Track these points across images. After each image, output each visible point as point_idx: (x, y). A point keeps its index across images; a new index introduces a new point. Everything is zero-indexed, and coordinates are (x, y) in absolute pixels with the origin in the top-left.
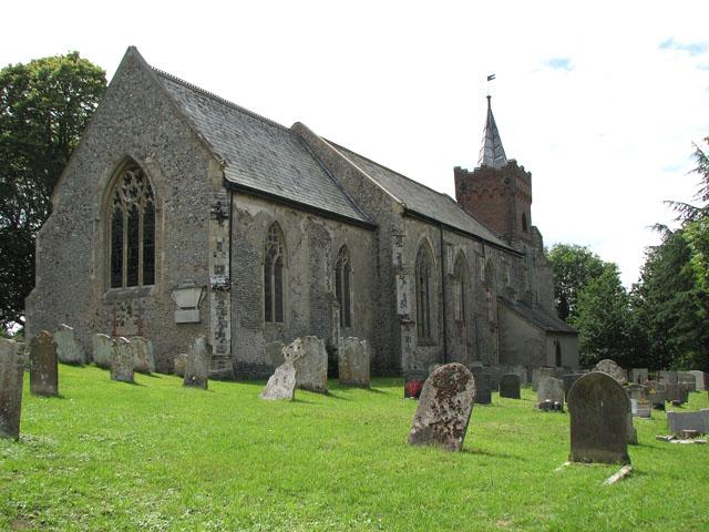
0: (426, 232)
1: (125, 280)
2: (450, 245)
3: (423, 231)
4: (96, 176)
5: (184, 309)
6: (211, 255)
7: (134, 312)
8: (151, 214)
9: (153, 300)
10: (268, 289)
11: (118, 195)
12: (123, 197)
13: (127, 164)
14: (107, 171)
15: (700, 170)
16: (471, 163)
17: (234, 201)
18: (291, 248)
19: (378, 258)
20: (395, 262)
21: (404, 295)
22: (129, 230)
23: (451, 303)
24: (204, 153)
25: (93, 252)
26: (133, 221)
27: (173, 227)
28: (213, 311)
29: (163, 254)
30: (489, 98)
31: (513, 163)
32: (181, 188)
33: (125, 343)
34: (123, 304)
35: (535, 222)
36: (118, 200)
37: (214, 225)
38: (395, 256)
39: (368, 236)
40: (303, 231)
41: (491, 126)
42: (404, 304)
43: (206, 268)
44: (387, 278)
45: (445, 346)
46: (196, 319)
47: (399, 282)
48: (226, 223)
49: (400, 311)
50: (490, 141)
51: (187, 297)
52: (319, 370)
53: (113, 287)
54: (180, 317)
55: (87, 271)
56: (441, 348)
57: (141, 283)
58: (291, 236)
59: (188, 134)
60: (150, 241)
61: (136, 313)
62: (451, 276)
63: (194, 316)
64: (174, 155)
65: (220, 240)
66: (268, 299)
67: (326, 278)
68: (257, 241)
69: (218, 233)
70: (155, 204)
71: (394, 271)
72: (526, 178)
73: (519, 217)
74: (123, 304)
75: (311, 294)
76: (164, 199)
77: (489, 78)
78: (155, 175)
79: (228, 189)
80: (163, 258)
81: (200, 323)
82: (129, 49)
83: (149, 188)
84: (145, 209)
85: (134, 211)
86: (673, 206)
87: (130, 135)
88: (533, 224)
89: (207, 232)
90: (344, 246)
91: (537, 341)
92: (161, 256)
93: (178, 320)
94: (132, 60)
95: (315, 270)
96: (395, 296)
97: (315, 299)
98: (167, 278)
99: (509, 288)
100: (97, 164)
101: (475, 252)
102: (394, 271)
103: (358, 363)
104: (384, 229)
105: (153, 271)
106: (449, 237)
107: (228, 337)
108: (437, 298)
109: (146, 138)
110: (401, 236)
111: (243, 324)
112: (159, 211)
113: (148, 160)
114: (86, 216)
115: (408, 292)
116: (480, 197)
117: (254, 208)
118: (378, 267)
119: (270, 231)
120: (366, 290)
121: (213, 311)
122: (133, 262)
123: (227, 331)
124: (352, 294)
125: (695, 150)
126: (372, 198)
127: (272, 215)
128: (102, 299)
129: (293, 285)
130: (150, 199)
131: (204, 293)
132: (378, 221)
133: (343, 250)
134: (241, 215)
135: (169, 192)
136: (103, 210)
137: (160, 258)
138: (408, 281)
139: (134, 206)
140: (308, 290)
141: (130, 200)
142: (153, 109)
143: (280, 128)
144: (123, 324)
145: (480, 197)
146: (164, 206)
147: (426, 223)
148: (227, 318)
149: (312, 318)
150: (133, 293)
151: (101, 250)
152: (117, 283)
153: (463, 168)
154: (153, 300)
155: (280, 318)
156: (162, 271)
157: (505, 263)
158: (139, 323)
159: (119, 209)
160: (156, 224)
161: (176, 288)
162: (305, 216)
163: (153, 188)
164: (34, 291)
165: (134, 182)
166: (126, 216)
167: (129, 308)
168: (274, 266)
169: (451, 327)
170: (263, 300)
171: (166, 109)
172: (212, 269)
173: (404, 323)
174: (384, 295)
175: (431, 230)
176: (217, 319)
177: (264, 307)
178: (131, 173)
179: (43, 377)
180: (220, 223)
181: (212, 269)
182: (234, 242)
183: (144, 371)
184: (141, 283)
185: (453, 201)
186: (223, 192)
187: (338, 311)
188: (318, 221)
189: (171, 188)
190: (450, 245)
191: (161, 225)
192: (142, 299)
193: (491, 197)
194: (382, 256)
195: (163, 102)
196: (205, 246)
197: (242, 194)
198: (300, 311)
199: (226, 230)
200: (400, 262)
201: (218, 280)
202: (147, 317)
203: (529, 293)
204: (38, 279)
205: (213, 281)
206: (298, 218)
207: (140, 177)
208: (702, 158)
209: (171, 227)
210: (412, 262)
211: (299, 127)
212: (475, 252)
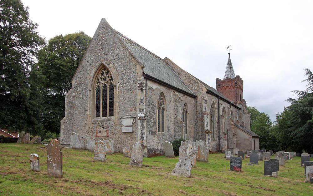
0: (214, 99)
2: (221, 104)
3: (213, 98)
5: (126, 126)
6: (138, 104)
7: (105, 127)
8: (112, 89)
9: (113, 122)
10: (159, 119)
11: (98, 80)
13: (102, 68)
14: (94, 70)
15: (310, 79)
16: (222, 78)
17: (147, 83)
18: (168, 103)
19: (197, 108)
20: (204, 110)
21: (207, 122)
22: (103, 94)
23: (221, 126)
24: (135, 62)
26: (105, 91)
27: (121, 92)
28: (139, 128)
29: (117, 104)
30: (229, 54)
31: (238, 77)
32: (125, 76)
33: (101, 143)
34: (100, 124)
35: (244, 98)
36: (99, 82)
38: (204, 108)
39: (193, 100)
40: (172, 97)
41: (230, 63)
43: (135, 110)
45: (219, 141)
47: (205, 117)
48: (144, 91)
49: (206, 128)
51: (129, 122)
53: (96, 117)
54: (124, 130)
55: (86, 110)
56: (217, 142)
58: (168, 98)
59: (128, 54)
60: (111, 99)
62: (222, 116)
63: (130, 129)
64: (122, 63)
65: (142, 98)
66: (159, 123)
67: (181, 115)
68: (156, 99)
69: (141, 95)
70: (114, 83)
71: (203, 114)
72: (242, 82)
73: (239, 96)
74: (100, 124)
75: (174, 121)
76: (118, 81)
78: (113, 72)
79: (145, 78)
80: (117, 106)
81: (133, 132)
82: (102, 19)
83: (111, 77)
84: (110, 86)
85: (105, 87)
87: (103, 55)
88: (243, 99)
89: (136, 95)
90: (186, 103)
91: (248, 140)
92: (116, 105)
94: (104, 26)
95: (176, 112)
96: (204, 123)
97: (176, 123)
98: (119, 114)
99: (237, 120)
100: (89, 67)
101: (228, 107)
102: (203, 114)
103: (203, 152)
104: (199, 98)
105: (113, 111)
106: (221, 102)
107: (145, 138)
108: (216, 123)
109: (110, 56)
111: (150, 133)
112: (115, 86)
113: (111, 65)
114: (85, 89)
116: (225, 89)
117: (155, 86)
118: (197, 112)
119: (160, 96)
120: (192, 120)
121: (139, 128)
122: (105, 107)
123: (145, 136)
124: (188, 122)
127: (161, 90)
129: (168, 118)
130: (111, 82)
131: (135, 120)
132: (197, 95)
133: (186, 104)
134: (150, 89)
135: (120, 78)
136: (92, 86)
137: (116, 105)
139: (105, 85)
140: (173, 120)
142: (113, 44)
143: (160, 59)
144: (100, 132)
145: (225, 89)
146: (118, 84)
147: (214, 96)
149: (174, 130)
151: (91, 103)
152: (98, 115)
154: (113, 122)
155: (163, 131)
157: (236, 111)
158: (107, 132)
159: (99, 86)
160: (114, 91)
162: (173, 91)
163: (113, 77)
164: (64, 118)
165: (105, 75)
168: (161, 110)
169: (221, 134)
170: (157, 123)
172: (138, 110)
174: (199, 122)
175: (215, 98)
176: (140, 131)
177: (157, 126)
178: (104, 71)
179: (54, 165)
181: (138, 110)
182: (147, 99)
185: (215, 90)
186: (143, 78)
187: (185, 128)
189: (120, 77)
190: (221, 104)
191: (116, 92)
192: (108, 122)
193: (230, 88)
195: (117, 41)
197: (150, 80)
198: (170, 128)
199: (144, 94)
200: (206, 110)
201: (141, 115)
202: (110, 129)
203: (243, 123)
204: (66, 113)
205: (139, 115)
206: (170, 91)
207: (108, 72)
208: (309, 72)
209: (120, 93)
210: (209, 110)
212: (228, 107)
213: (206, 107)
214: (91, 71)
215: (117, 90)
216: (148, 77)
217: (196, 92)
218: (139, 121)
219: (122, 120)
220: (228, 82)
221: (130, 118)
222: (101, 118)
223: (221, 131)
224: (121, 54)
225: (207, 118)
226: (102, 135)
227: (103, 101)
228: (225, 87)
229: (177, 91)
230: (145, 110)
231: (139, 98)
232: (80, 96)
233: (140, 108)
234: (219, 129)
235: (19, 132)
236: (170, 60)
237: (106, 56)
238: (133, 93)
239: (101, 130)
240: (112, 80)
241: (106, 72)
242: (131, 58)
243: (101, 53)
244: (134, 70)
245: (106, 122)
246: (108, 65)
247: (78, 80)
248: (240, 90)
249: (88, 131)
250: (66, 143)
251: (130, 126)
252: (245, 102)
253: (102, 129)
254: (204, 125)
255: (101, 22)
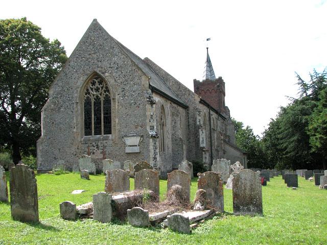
1: (93, 132)
4: (76, 81)
5: (130, 146)
6: (148, 121)
8: (108, 101)
12: (91, 91)
13: (93, 76)
16: (201, 78)
20: (198, 123)
21: (203, 138)
22: (95, 108)
25: (75, 118)
30: (207, 48)
31: (220, 79)
34: (94, 143)
37: (148, 106)
38: (198, 120)
41: (209, 61)
42: (203, 142)
44: (193, 130)
46: (138, 151)
47: (201, 132)
49: (201, 146)
50: (208, 68)
52: (225, 174)
53: (85, 135)
54: (128, 150)
55: (71, 127)
57: (103, 133)
59: (130, 63)
61: (102, 148)
63: (137, 150)
64: (122, 73)
65: (152, 114)
77: (208, 40)
78: (111, 82)
80: (117, 122)
83: (107, 88)
85: (97, 98)
86: (289, 98)
87: (96, 61)
91: (239, 158)
93: (126, 152)
96: (199, 139)
100: (76, 75)
102: (197, 128)
104: (191, 108)
109: (105, 64)
110: (200, 112)
113: (107, 74)
115: (204, 137)
116: (205, 93)
118: (188, 125)
125: (296, 75)
126: (185, 94)
128: (81, 141)
131: (142, 139)
132: (188, 105)
135: (120, 90)
137: (115, 121)
138: (204, 132)
139: (97, 96)
141: (95, 93)
143: (139, 59)
145: (205, 93)
146: (117, 97)
148: (158, 151)
149: (173, 149)
150: (99, 138)
152: (90, 134)
153: (197, 80)
156: (117, 128)
158: (103, 153)
161: (126, 136)
165: (97, 85)
166: (93, 101)
167: (97, 145)
171: (117, 50)
173: (204, 151)
180: (152, 106)
181: (148, 128)
183: (92, 174)
184: (103, 133)
186: (150, 91)
188: (175, 105)
189: (120, 88)
191: (115, 107)
192: (105, 141)
194: (190, 120)
196: (145, 115)
202: (108, 150)
205: (150, 133)
211: (147, 59)
213: (200, 120)
214: (78, 79)
215: (117, 103)
216: (154, 90)
217: (187, 101)
218: (151, 140)
219: (125, 138)
220: (209, 84)
221: (136, 137)
222: (93, 137)
223: (213, 148)
224: (120, 63)
225: (203, 132)
226: (97, 157)
227: (94, 116)
228: (205, 91)
229: (174, 103)
230: (155, 128)
231: (148, 113)
232: (62, 109)
233: (151, 125)
234: (211, 146)
235: (264, 149)
236: (151, 61)
237: (100, 63)
238: (139, 107)
239: (95, 151)
240: (108, 91)
241: (98, 82)
242: (134, 68)
243: (93, 59)
244: (139, 81)
245: (102, 142)
246: (103, 73)
247: (58, 89)
248: (222, 95)
249: (75, 153)
250: (45, 169)
251: (136, 146)
252: (228, 109)
253: (96, 149)
254: (199, 141)
255: (92, 23)
